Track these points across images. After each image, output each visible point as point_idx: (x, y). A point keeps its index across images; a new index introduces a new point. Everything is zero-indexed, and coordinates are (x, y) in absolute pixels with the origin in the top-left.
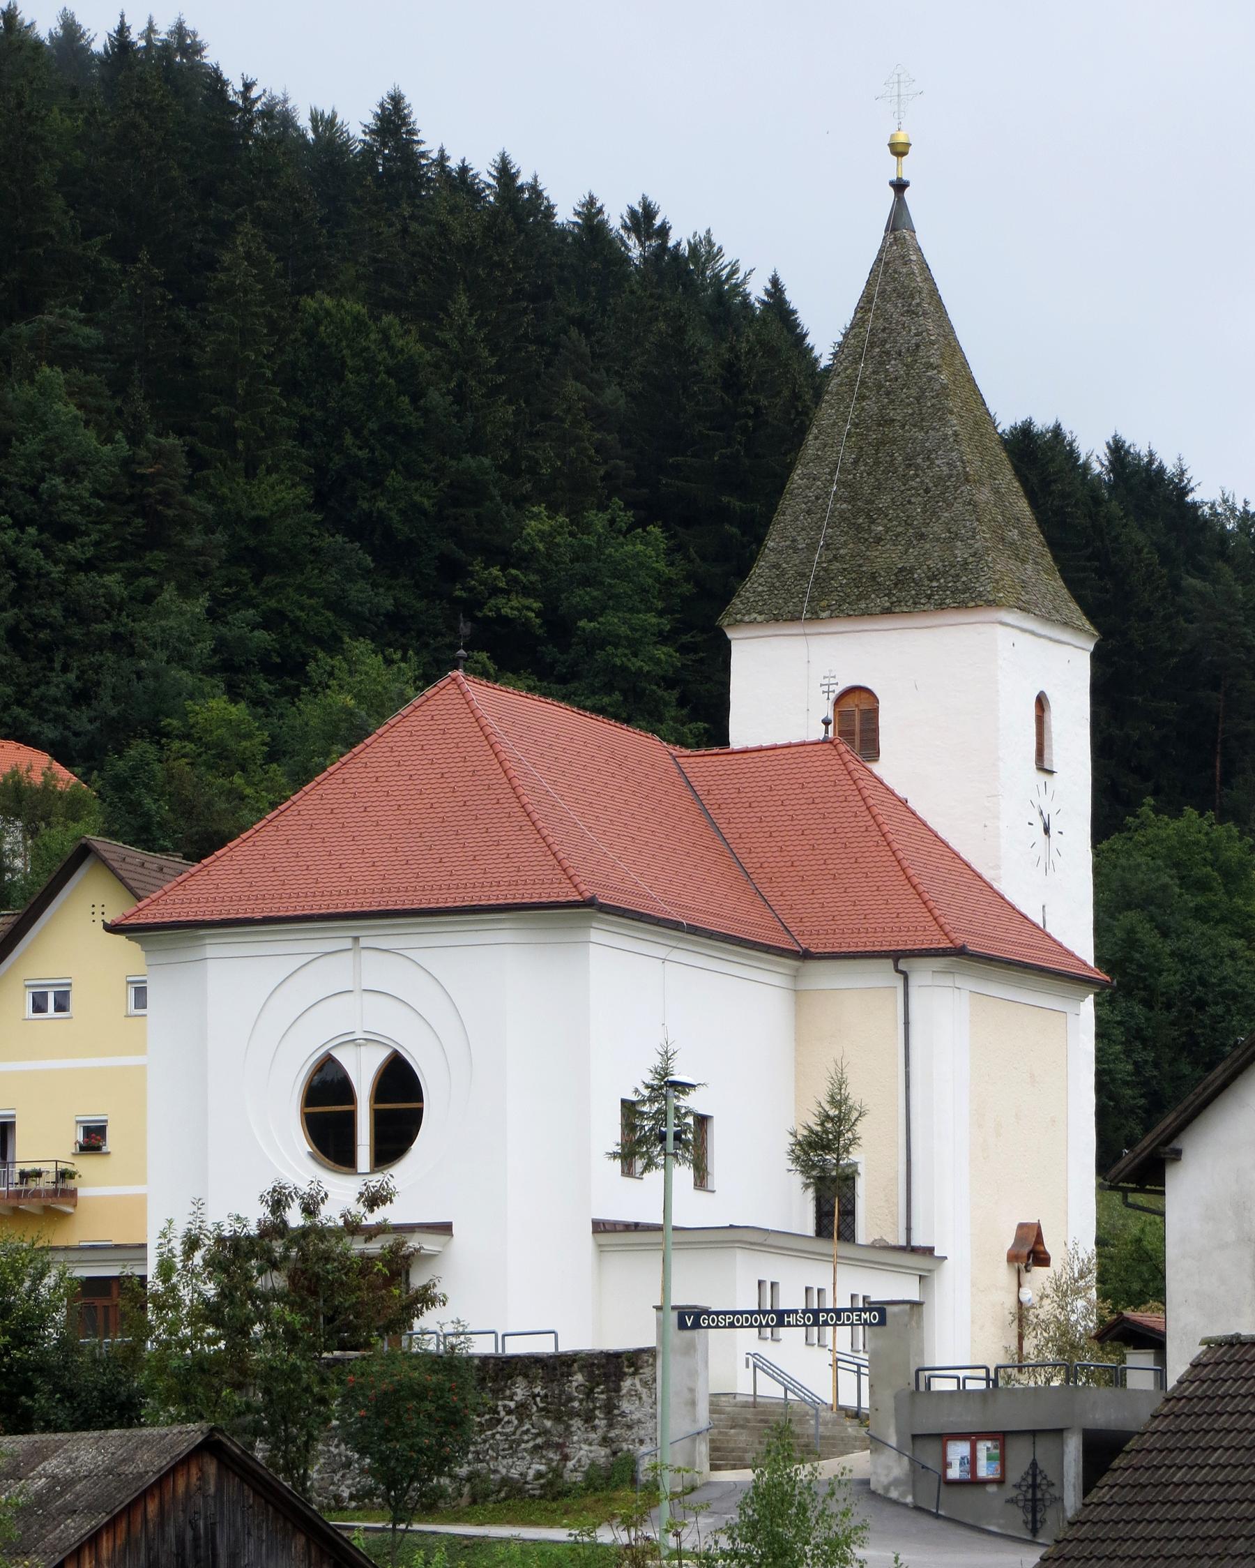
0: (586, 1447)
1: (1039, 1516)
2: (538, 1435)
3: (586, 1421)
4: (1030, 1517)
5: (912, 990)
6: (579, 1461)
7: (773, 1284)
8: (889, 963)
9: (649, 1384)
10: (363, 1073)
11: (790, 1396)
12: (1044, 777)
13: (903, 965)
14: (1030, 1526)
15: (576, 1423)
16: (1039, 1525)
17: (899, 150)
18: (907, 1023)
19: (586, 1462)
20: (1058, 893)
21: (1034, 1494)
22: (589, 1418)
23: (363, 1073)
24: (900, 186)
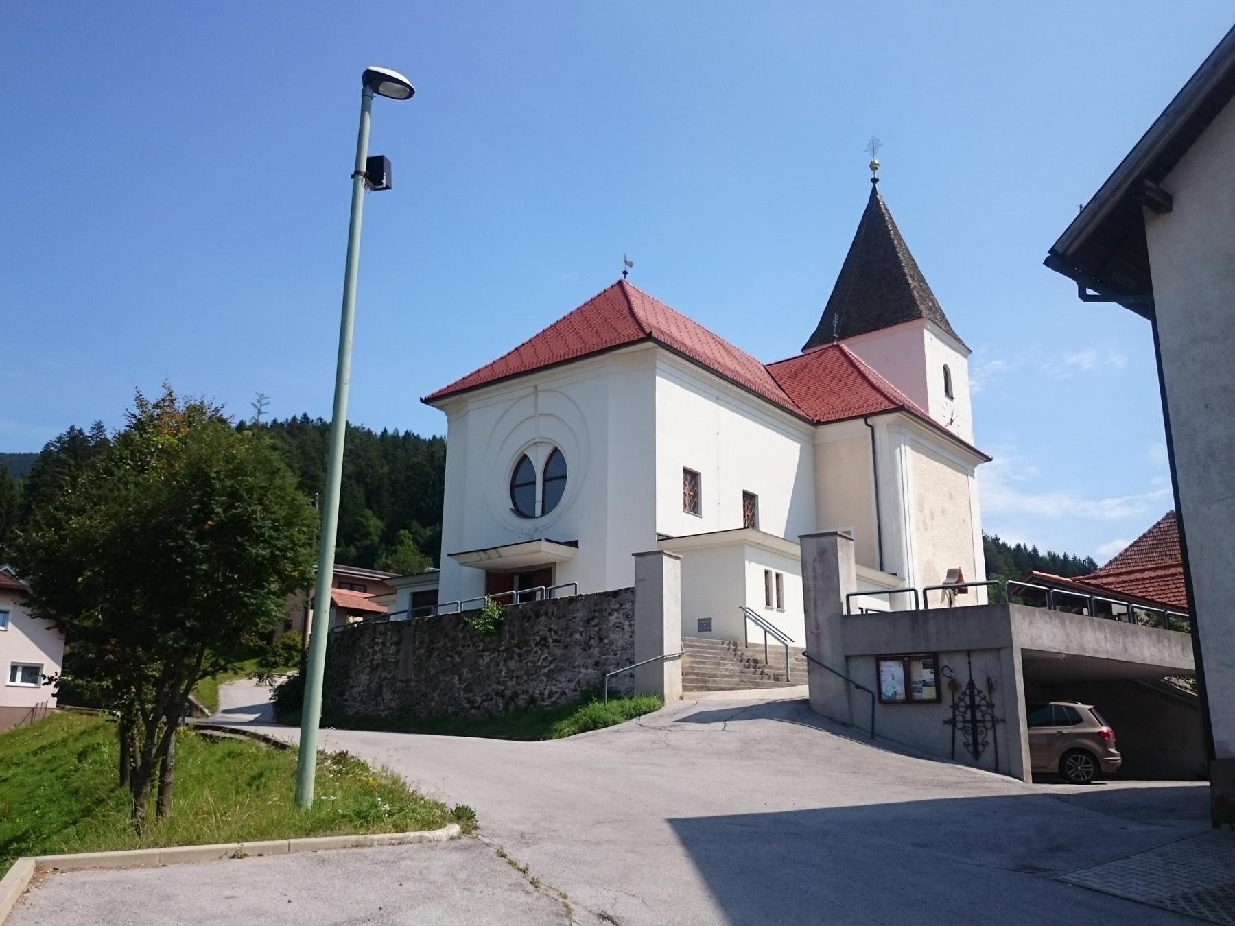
0: (583, 670)
1: (980, 738)
2: (551, 662)
3: (584, 650)
4: (970, 739)
5: (949, 746)
6: (579, 682)
7: (777, 576)
8: (863, 421)
9: (629, 616)
10: (539, 462)
11: (772, 641)
12: (948, 400)
13: (869, 421)
14: (971, 749)
15: (578, 650)
16: (981, 748)
17: (874, 167)
18: (874, 452)
19: (583, 682)
20: (957, 604)
21: (973, 715)
22: (586, 647)
23: (539, 462)
24: (875, 181)
